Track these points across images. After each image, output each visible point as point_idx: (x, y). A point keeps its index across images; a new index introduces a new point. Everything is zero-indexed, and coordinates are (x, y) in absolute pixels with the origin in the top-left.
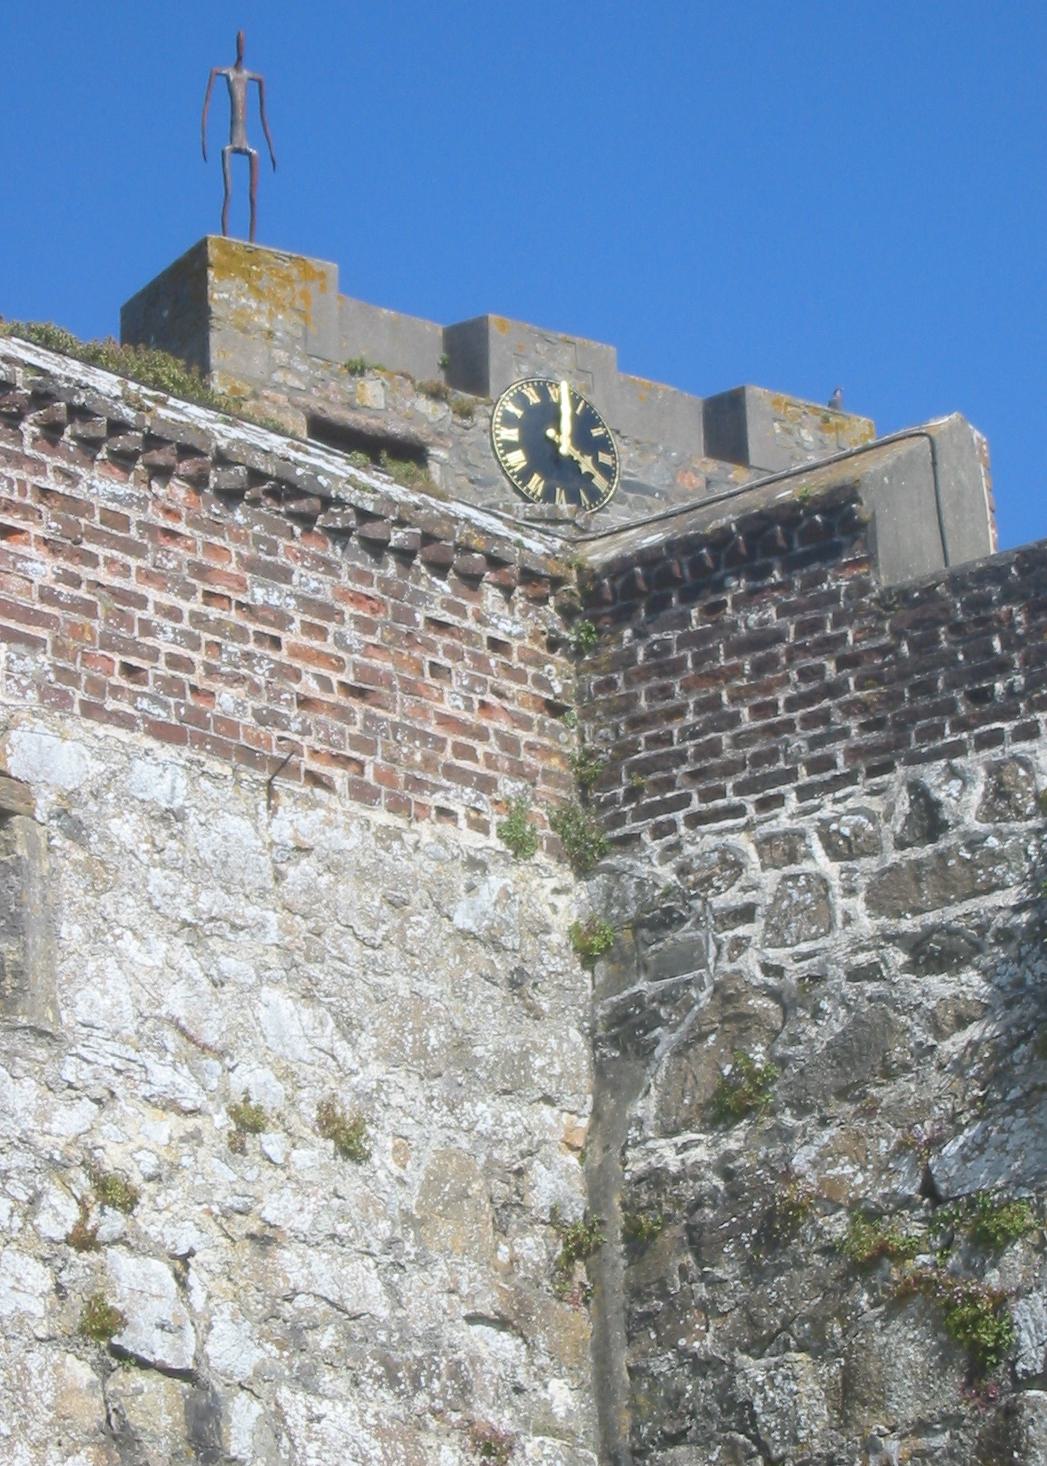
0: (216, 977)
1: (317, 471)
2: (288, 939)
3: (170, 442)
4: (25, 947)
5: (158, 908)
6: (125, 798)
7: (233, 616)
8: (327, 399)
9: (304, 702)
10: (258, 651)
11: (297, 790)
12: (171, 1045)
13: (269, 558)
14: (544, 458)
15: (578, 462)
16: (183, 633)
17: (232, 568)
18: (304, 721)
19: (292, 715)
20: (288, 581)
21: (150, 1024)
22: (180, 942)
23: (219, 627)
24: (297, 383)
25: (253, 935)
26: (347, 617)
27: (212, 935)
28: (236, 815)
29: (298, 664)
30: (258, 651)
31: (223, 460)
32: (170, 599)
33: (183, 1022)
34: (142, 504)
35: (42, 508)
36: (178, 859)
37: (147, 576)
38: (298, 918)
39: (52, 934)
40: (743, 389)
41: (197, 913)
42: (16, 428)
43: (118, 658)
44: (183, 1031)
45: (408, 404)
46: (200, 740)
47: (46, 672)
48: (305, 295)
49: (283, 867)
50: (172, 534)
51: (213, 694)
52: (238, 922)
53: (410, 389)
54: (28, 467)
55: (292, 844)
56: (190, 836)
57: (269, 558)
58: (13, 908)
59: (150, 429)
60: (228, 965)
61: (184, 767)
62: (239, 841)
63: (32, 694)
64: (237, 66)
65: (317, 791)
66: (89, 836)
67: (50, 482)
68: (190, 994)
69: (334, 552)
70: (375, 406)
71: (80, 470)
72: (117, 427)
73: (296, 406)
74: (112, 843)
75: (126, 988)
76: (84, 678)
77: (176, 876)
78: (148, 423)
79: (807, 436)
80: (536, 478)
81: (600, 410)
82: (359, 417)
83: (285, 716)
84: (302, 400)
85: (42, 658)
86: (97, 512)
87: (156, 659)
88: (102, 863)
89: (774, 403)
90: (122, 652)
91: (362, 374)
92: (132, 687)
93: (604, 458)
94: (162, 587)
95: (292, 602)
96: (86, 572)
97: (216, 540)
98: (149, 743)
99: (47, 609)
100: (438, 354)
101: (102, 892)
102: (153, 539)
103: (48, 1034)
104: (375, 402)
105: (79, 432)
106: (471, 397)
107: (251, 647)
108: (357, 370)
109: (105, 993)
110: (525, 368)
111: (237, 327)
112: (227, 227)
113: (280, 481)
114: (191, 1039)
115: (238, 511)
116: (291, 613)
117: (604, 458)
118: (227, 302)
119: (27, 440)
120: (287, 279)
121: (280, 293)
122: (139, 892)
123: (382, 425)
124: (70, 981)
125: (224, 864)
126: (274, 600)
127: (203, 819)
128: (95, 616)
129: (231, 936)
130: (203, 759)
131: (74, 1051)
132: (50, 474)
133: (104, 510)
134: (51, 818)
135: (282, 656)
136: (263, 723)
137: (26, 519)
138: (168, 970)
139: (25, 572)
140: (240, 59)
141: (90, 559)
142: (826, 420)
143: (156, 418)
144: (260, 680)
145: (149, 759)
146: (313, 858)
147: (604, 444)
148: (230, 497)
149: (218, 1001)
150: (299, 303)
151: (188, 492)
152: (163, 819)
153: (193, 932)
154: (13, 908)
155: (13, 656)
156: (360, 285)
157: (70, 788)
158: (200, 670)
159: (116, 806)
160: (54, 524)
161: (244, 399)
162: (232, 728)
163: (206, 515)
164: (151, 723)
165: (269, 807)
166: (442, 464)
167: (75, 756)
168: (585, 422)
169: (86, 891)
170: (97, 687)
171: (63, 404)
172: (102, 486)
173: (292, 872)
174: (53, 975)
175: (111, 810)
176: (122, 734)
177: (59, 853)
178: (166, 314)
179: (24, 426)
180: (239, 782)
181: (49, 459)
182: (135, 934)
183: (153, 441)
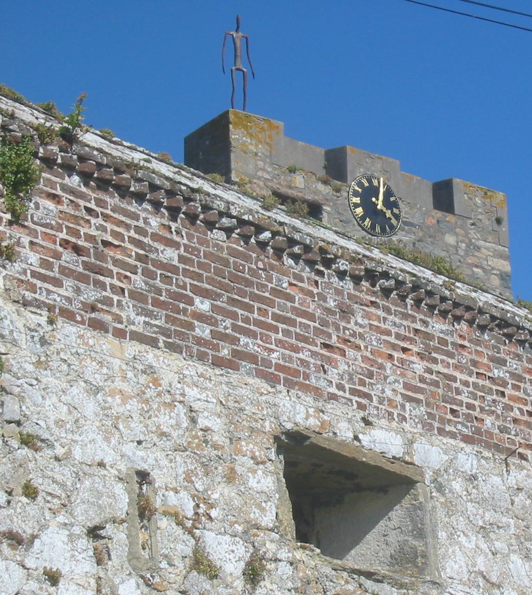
0: (494, 551)
1: (515, 314)
2: (518, 531)
3: (463, 305)
4: (426, 544)
5: (471, 521)
6: (456, 470)
7: (487, 383)
8: (280, 184)
9: (515, 421)
10: (498, 399)
11: (516, 461)
12: (481, 584)
13: (498, 355)
14: (371, 210)
15: (385, 213)
16: (471, 393)
17: (485, 361)
18: (516, 430)
19: (511, 427)
20: (506, 366)
21: (473, 575)
22: (480, 536)
23: (482, 389)
24: (267, 177)
25: (505, 531)
26: (527, 380)
27: (490, 531)
28: (496, 475)
29: (512, 404)
30: (498, 399)
31: (481, 312)
32: (464, 377)
33: (485, 573)
34: (451, 333)
35: (416, 338)
36: (477, 498)
37: (456, 367)
38: (520, 521)
39: (436, 537)
40: (452, 179)
41: (484, 522)
42: (405, 301)
43: (449, 406)
44: (484, 577)
45: (314, 186)
46: (480, 442)
47: (424, 415)
48: (270, 137)
49: (513, 498)
50: (463, 347)
51: (483, 420)
52: (500, 525)
53: (315, 179)
54: (410, 319)
55: (516, 487)
56: (480, 487)
57: (498, 355)
58: (420, 525)
59: (455, 299)
60: (498, 545)
61: (475, 455)
62: (497, 487)
63: (419, 426)
64: (237, 31)
65: (523, 461)
66: (445, 490)
67: (418, 326)
68: (486, 560)
69: (520, 351)
70: (300, 187)
71: (429, 320)
72: (443, 299)
73: (267, 187)
74: (453, 493)
75: (463, 560)
76: (437, 416)
77: (477, 505)
78: (454, 297)
79: (478, 201)
80: (368, 220)
81: (393, 188)
82: (294, 192)
83: (509, 428)
84: (270, 184)
85: (422, 409)
86: (436, 338)
87: (462, 406)
88: (450, 502)
89: (465, 186)
90: (451, 403)
91: (294, 173)
92: (455, 419)
93: (396, 211)
94: (462, 372)
95: (507, 375)
96: (435, 367)
97: (478, 348)
98: (462, 445)
99: (422, 386)
100: (322, 162)
101: (452, 516)
102: (457, 350)
103: (437, 583)
104: (300, 185)
105: (428, 302)
106: (340, 183)
107: (495, 397)
108: (292, 170)
109: (456, 562)
110: (362, 170)
111: (242, 150)
112: (234, 104)
113: (501, 320)
114: (487, 581)
115: (486, 335)
116: (508, 380)
117: (396, 211)
118: (238, 139)
119: (409, 307)
120: (263, 129)
121: (260, 136)
122: (464, 515)
123: (303, 196)
124: (443, 558)
125: (493, 498)
126: (501, 375)
127: (484, 478)
128: (439, 388)
129: (497, 531)
130: (482, 450)
131: (447, 591)
132: (418, 322)
133: (439, 337)
134: (431, 483)
135: (506, 400)
136: (501, 432)
137: (411, 344)
138: (477, 549)
139: (413, 369)
140: (238, 27)
141: (435, 361)
142: (486, 194)
143: (457, 294)
144: (499, 412)
145: (463, 452)
146: (523, 493)
147: (395, 205)
148: (482, 328)
149: (496, 562)
150: (268, 140)
151: (467, 327)
152: (470, 479)
153: (484, 531)
154: (420, 525)
155: (412, 409)
156: (293, 133)
157: (437, 468)
158: (478, 409)
159: (453, 475)
160: (421, 346)
161: (246, 184)
162: (491, 435)
163: (474, 337)
164: (463, 435)
165: (507, 471)
166: (328, 213)
167: (438, 454)
168: (388, 193)
169: (445, 515)
170: (442, 420)
171: (423, 290)
172: (438, 326)
173: (516, 499)
174: (437, 556)
175: (452, 477)
176: (452, 441)
177: (435, 499)
178: (207, 143)
179: (408, 300)
180: (495, 460)
181: (417, 315)
182: (464, 534)
183: (456, 305)
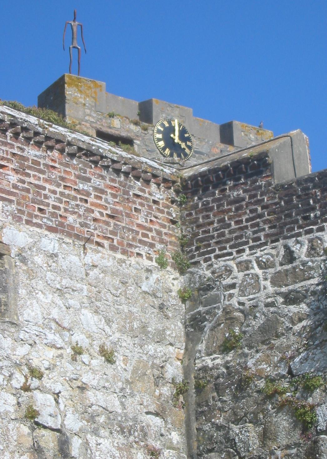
0: (67, 306)
1: (99, 147)
2: (90, 294)
3: (53, 138)
4: (8, 296)
5: (49, 284)
6: (39, 250)
7: (73, 193)
8: (102, 125)
9: (95, 220)
10: (81, 204)
11: (93, 247)
12: (53, 327)
13: (84, 175)
14: (170, 143)
15: (180, 145)
16: (57, 198)
17: (72, 178)
18: (95, 226)
19: (91, 224)
20: (90, 182)
21: (47, 321)
22: (56, 295)
23: (68, 196)
24: (93, 120)
25: (79, 293)
26: (108, 193)
27: (66, 293)
28: (74, 255)
29: (93, 208)
30: (81, 204)
31: (70, 144)
32: (53, 188)
33: (57, 320)
34: (44, 158)
35: (13, 159)
36: (56, 269)
37: (46, 180)
38: (93, 287)
39: (16, 292)
40: (232, 122)
41: (61, 286)
42: (5, 134)
43: (37, 206)
44: (57, 323)
45: (128, 126)
46: (63, 232)
47: (15, 211)
48: (95, 92)
49: (88, 271)
50: (54, 167)
51: (66, 217)
52: (74, 289)
53: (128, 122)
54: (9, 146)
55: (91, 264)
56: (59, 262)
57: (84, 175)
58: (4, 284)
59: (47, 134)
60: (71, 302)
61: (57, 240)
62: (75, 263)
63: (10, 217)
64: (74, 21)
65: (99, 248)
66: (28, 262)
67: (16, 151)
68: (59, 311)
69: (104, 173)
70: (117, 127)
71: (25, 147)
72: (37, 134)
73: (93, 127)
74: (35, 264)
75: (39, 309)
76: (26, 212)
77: (55, 274)
78: (46, 132)
79: (252, 137)
80: (167, 150)
81: (188, 128)
82: (112, 131)
83: (89, 224)
84: (94, 125)
85: (13, 206)
86: (30, 160)
87: (49, 206)
88: (32, 270)
89: (242, 126)
90: (38, 204)
91: (113, 117)
92: (41, 215)
93: (189, 143)
94: (51, 184)
95: (91, 188)
96: (27, 179)
97: (67, 169)
98: (47, 232)
99: (15, 191)
100: (137, 111)
101: (32, 279)
102: (48, 169)
103: (15, 324)
104: (117, 126)
105: (25, 135)
106: (147, 124)
107: (78, 202)
108: (111, 116)
109: (33, 311)
110: (164, 115)
111: (74, 102)
112: (71, 71)
113: (87, 150)
114: (60, 325)
115: (74, 160)
116: (91, 192)
117: (189, 143)
118: (71, 95)
119: (9, 138)
120: (90, 87)
121: (87, 92)
122: (43, 279)
123: (119, 133)
124: (22, 307)
125: (70, 270)
126: (86, 188)
127: (63, 256)
128: (30, 193)
129: (72, 293)
130: (63, 238)
131: (23, 329)
132: (16, 148)
133: (33, 160)
134: (16, 256)
135: (88, 205)
136: (82, 226)
137: (8, 163)
138: (52, 304)
139: (8, 179)
140: (75, 18)
141: (28, 175)
142: (258, 132)
143: (49, 131)
144: (81, 213)
145: (46, 238)
146: (98, 269)
147: (189, 139)
148: (72, 156)
149: (68, 313)
150: (93, 95)
151: (59, 154)
152: (51, 256)
153: (60, 292)
154: (4, 284)
155: (4, 206)
156: (112, 89)
157: (22, 247)
158: (62, 210)
159: (36, 252)
160: (17, 164)
161: (76, 125)
162: (73, 228)
163: (64, 161)
164: (47, 226)
165: (84, 253)
166: (138, 145)
167: (23, 237)
168: (183, 132)
169: (27, 279)
170: (30, 215)
171: (20, 127)
172: (32, 152)
173: (91, 273)
174: (17, 305)
175: (35, 254)
176: (38, 230)
177: (18, 267)
178: (52, 98)
179: (7, 133)
180: (75, 245)
181: (15, 144)
182: (42, 292)
183: (48, 138)
